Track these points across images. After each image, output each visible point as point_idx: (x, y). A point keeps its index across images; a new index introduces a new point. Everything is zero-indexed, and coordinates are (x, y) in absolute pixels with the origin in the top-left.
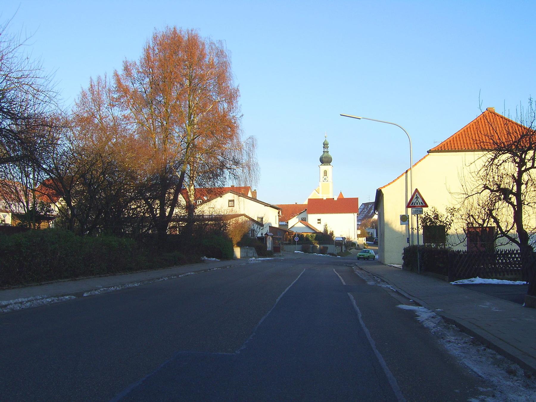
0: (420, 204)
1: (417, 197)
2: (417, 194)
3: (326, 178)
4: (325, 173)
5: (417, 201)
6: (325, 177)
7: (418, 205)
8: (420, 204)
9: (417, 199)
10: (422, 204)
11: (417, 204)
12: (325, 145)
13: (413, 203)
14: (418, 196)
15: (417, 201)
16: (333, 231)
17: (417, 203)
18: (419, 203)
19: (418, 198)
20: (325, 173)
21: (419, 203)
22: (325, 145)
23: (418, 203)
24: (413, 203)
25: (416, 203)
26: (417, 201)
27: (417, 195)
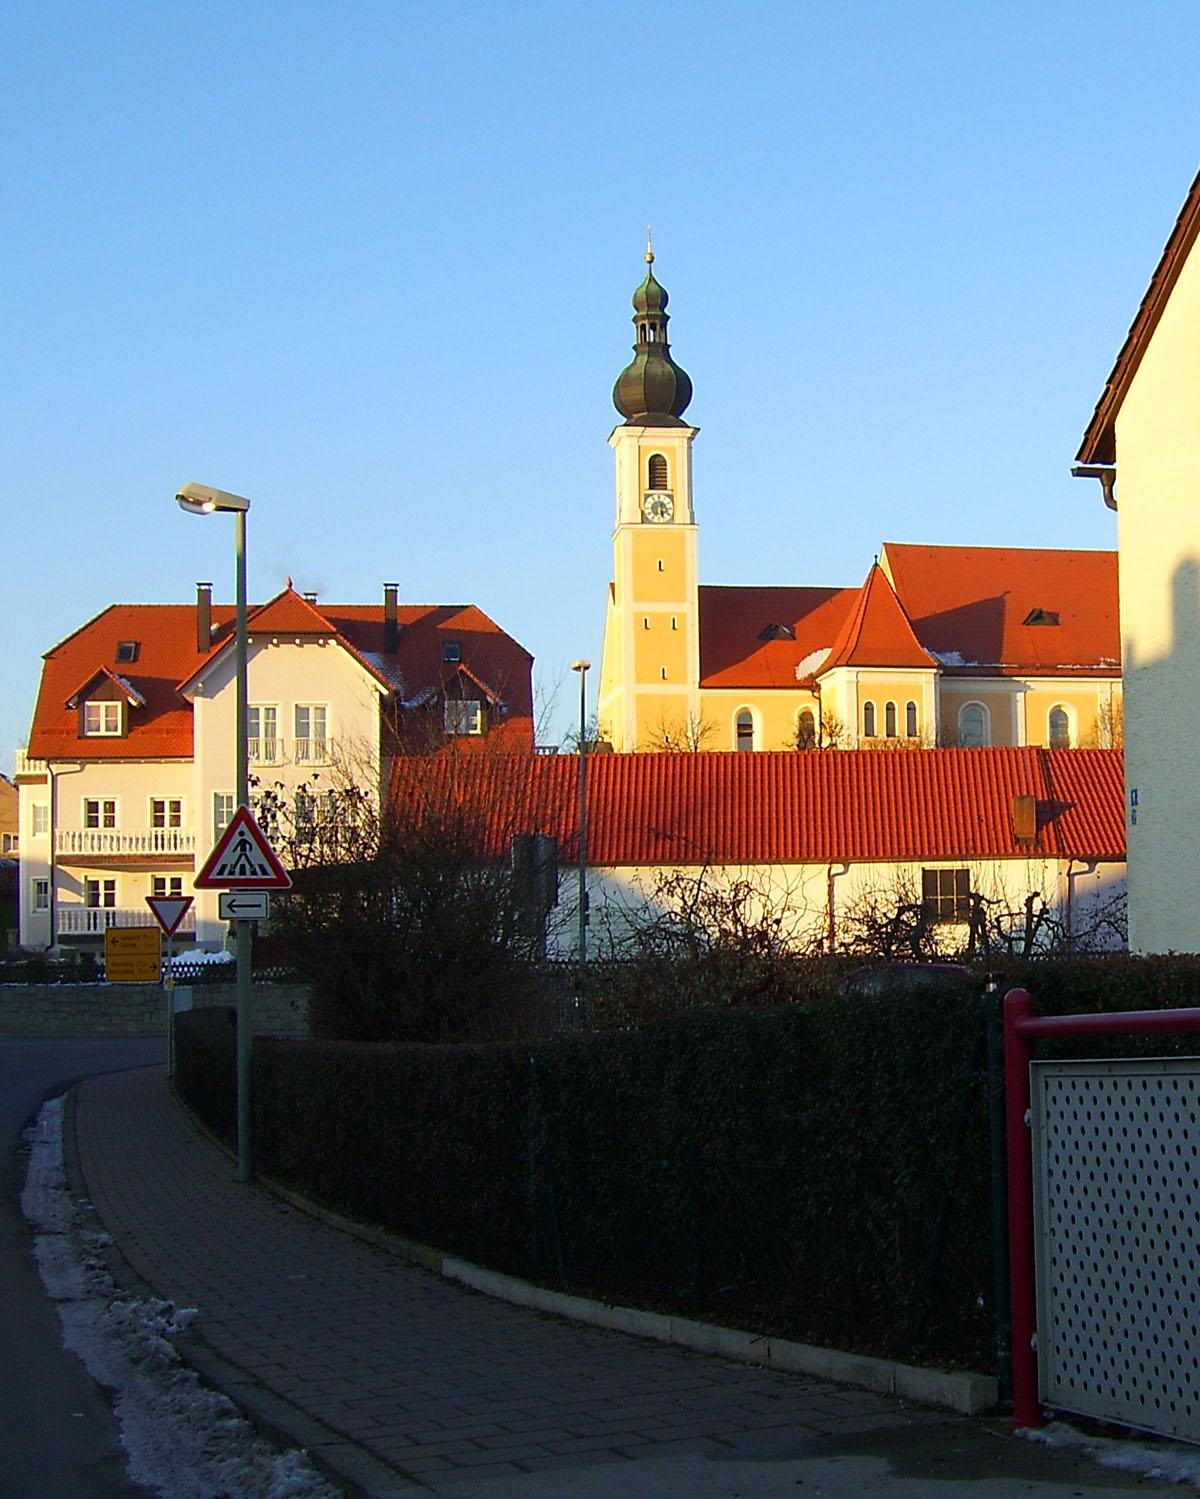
0: (254, 873)
1: (243, 843)
2: (246, 830)
3: (667, 501)
4: (657, 472)
5: (243, 857)
6: (658, 495)
7: (248, 876)
8: (254, 873)
9: (243, 849)
10: (264, 872)
11: (243, 872)
12: (653, 308)
13: (224, 867)
14: (249, 837)
15: (243, 857)
16: (138, 645)
17: (243, 866)
18: (251, 866)
19: (248, 846)
20: (657, 472)
21: (251, 866)
22: (653, 308)
23: (248, 867)
24: (224, 867)
25: (238, 869)
26: (243, 860)
27: (242, 834)
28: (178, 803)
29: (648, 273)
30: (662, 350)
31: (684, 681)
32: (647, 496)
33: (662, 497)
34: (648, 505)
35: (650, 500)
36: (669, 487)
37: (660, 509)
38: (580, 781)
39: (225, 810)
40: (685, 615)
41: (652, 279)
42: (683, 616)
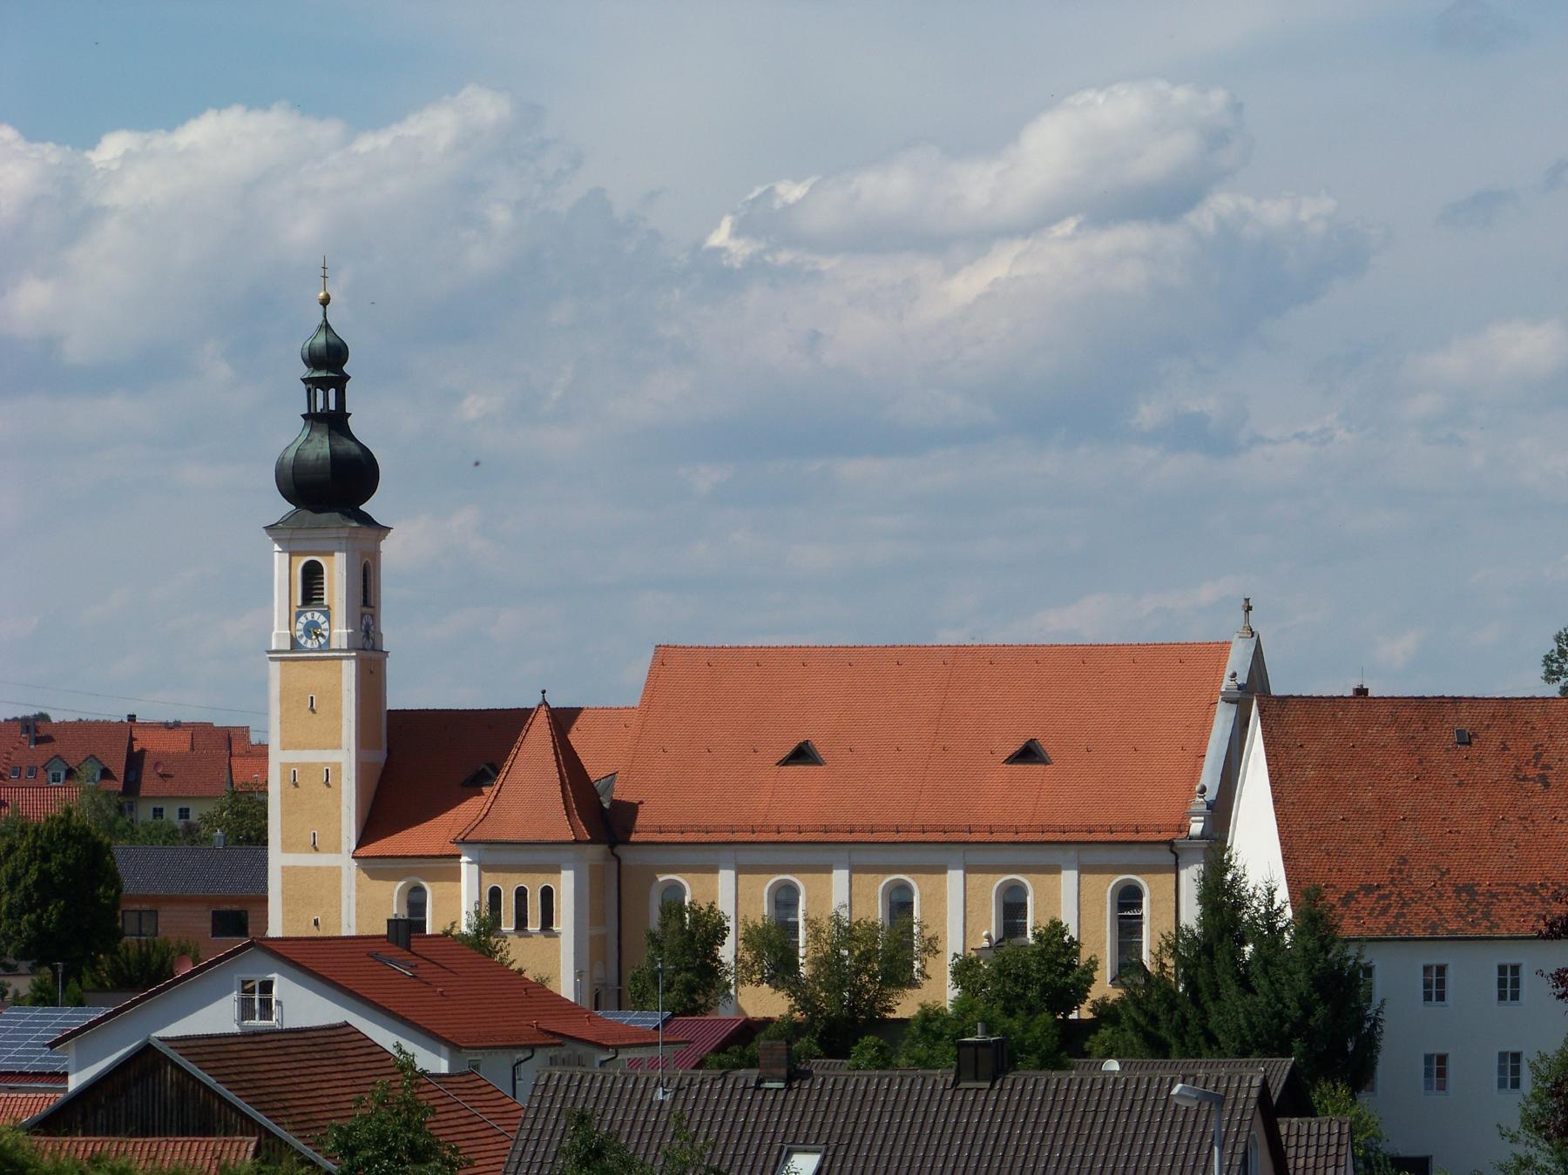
3: (322, 619)
28: (1442, 1059)
29: (322, 318)
30: (334, 422)
31: (337, 850)
32: (299, 615)
33: (317, 615)
34: (300, 626)
35: (303, 619)
36: (325, 602)
37: (312, 629)
38: (439, 984)
39: (257, 996)
40: (340, 764)
41: (326, 327)
42: (338, 767)
